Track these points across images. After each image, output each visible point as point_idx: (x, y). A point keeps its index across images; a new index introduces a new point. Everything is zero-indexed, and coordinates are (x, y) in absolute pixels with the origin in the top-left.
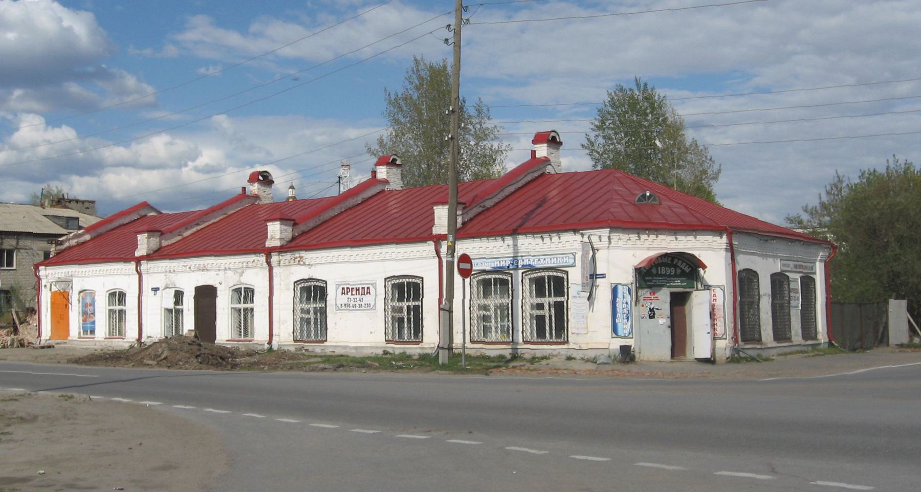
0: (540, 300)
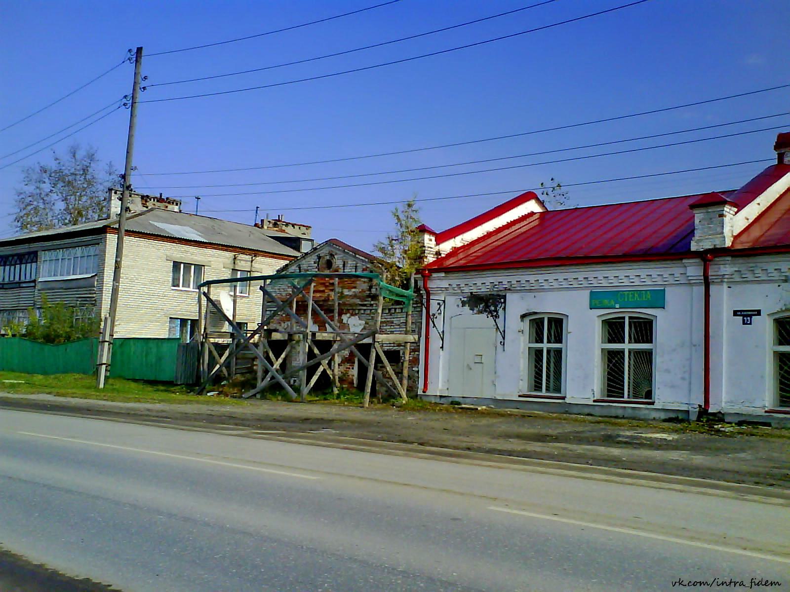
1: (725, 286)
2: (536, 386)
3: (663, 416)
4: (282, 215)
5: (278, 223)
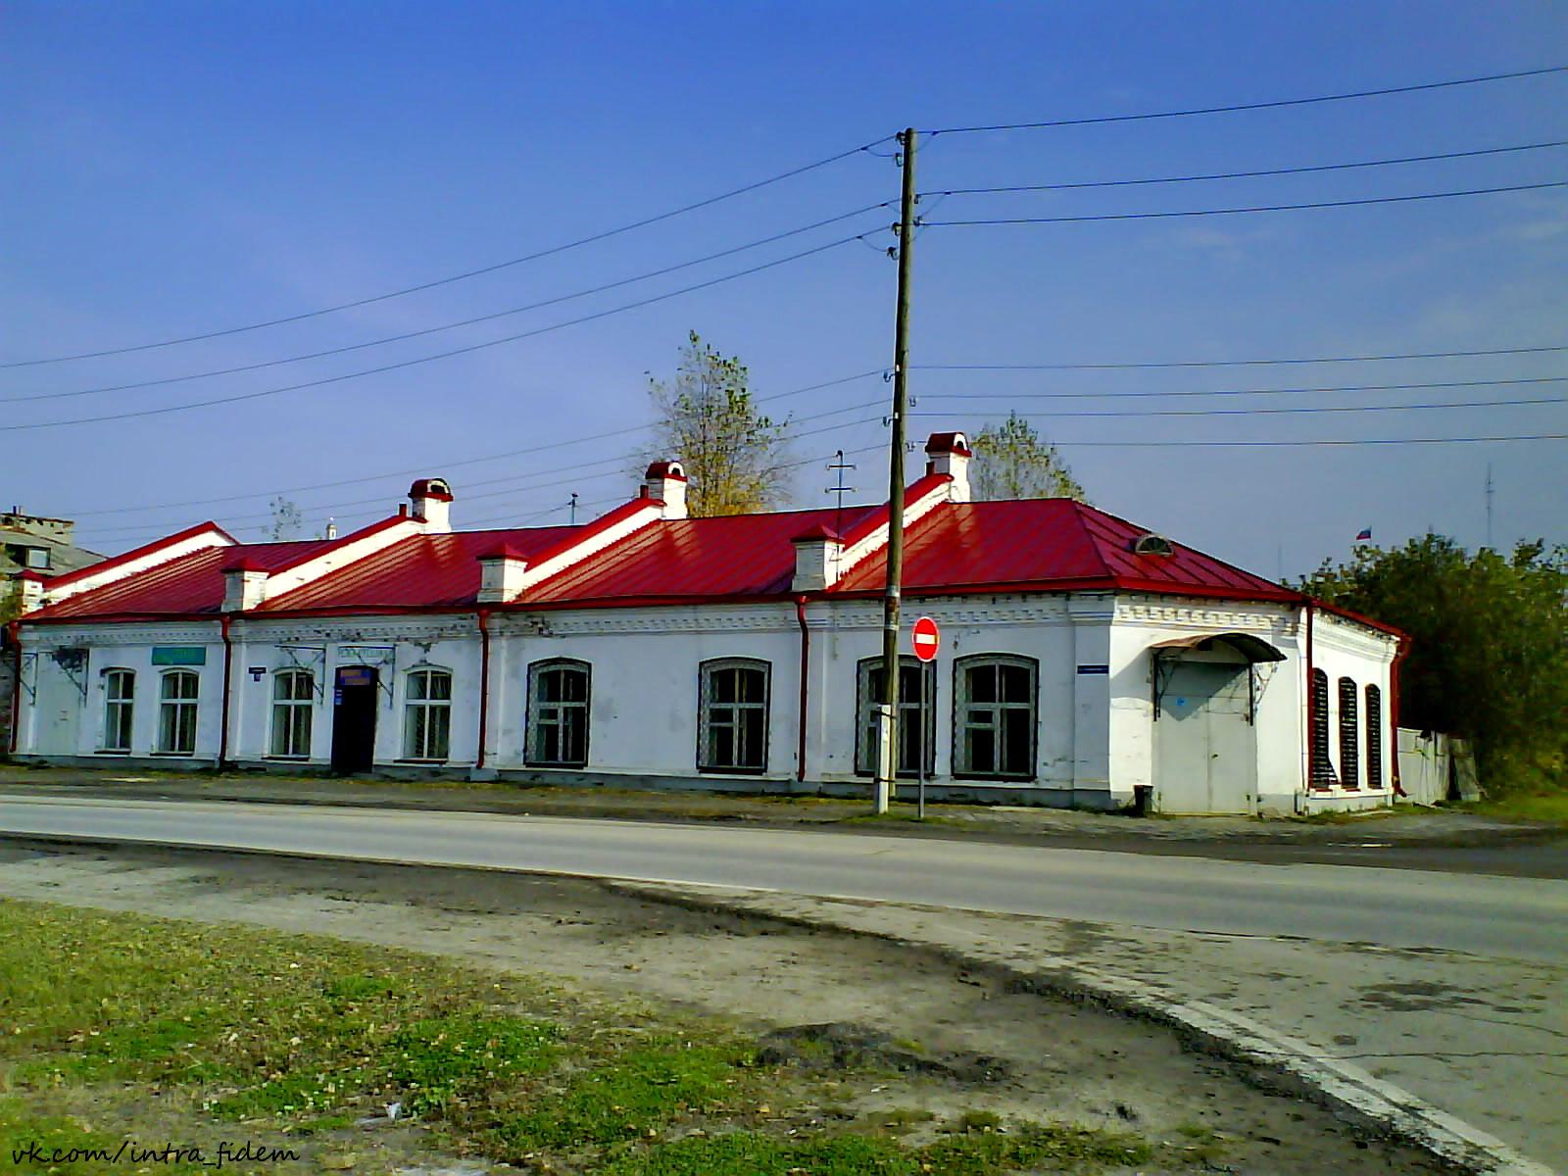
0: (552, 705)
1: (244, 646)
2: (417, 752)
3: (199, 766)
4: (20, 507)
5: (13, 518)
